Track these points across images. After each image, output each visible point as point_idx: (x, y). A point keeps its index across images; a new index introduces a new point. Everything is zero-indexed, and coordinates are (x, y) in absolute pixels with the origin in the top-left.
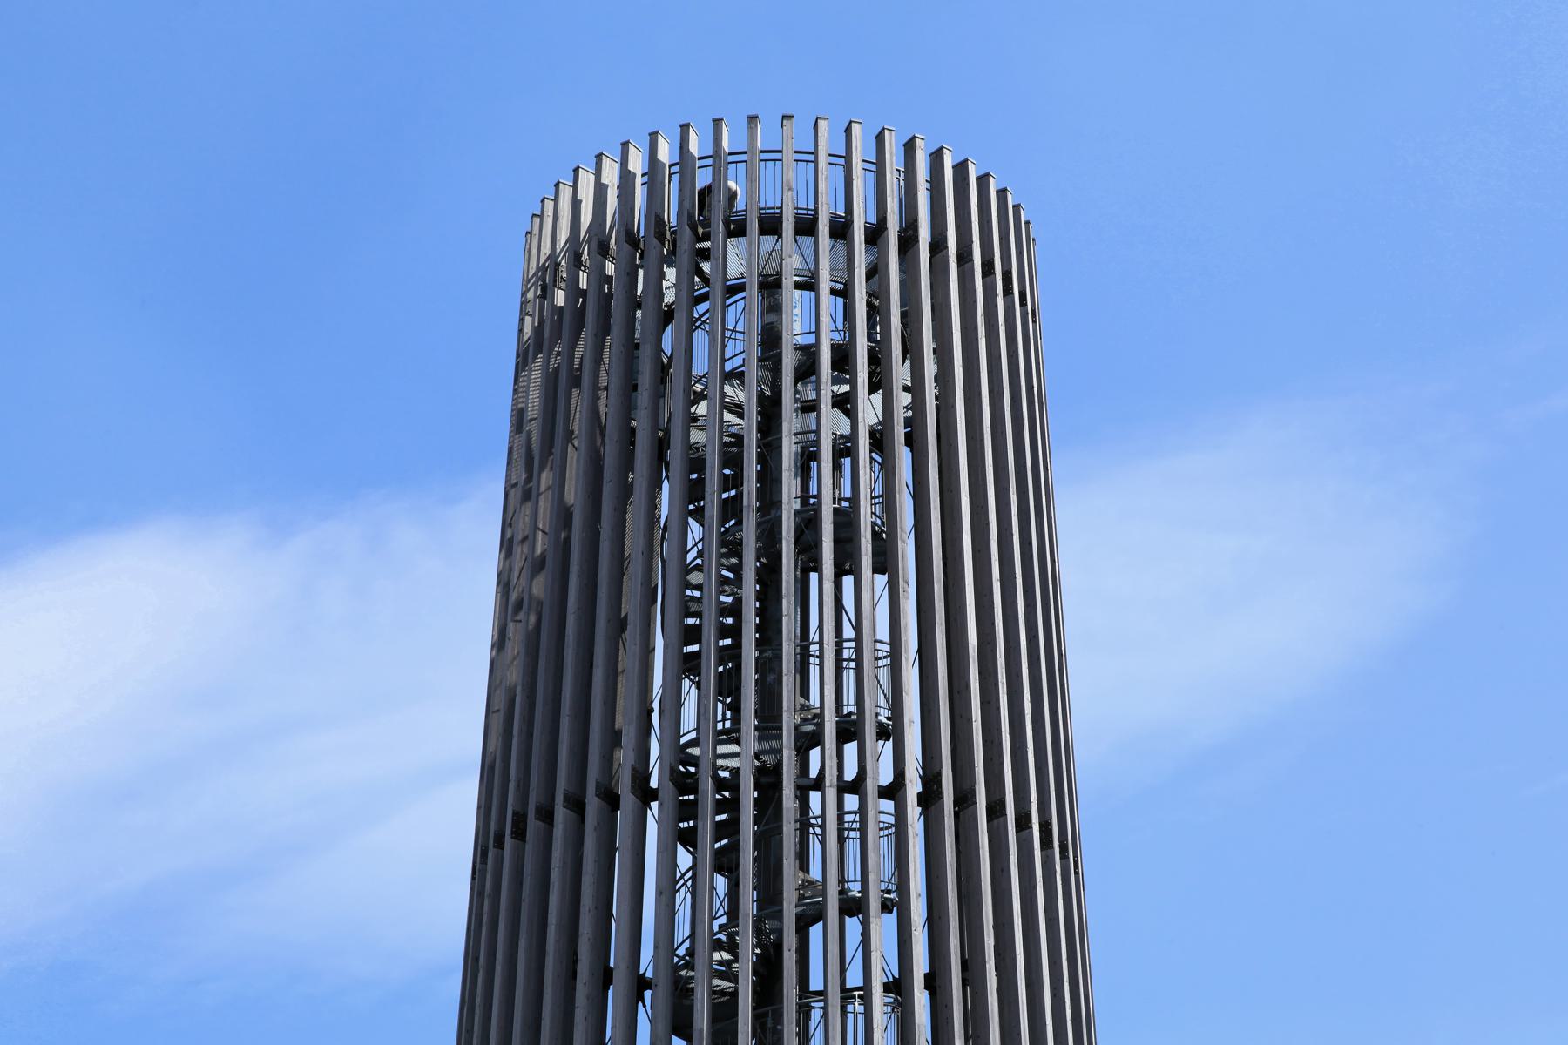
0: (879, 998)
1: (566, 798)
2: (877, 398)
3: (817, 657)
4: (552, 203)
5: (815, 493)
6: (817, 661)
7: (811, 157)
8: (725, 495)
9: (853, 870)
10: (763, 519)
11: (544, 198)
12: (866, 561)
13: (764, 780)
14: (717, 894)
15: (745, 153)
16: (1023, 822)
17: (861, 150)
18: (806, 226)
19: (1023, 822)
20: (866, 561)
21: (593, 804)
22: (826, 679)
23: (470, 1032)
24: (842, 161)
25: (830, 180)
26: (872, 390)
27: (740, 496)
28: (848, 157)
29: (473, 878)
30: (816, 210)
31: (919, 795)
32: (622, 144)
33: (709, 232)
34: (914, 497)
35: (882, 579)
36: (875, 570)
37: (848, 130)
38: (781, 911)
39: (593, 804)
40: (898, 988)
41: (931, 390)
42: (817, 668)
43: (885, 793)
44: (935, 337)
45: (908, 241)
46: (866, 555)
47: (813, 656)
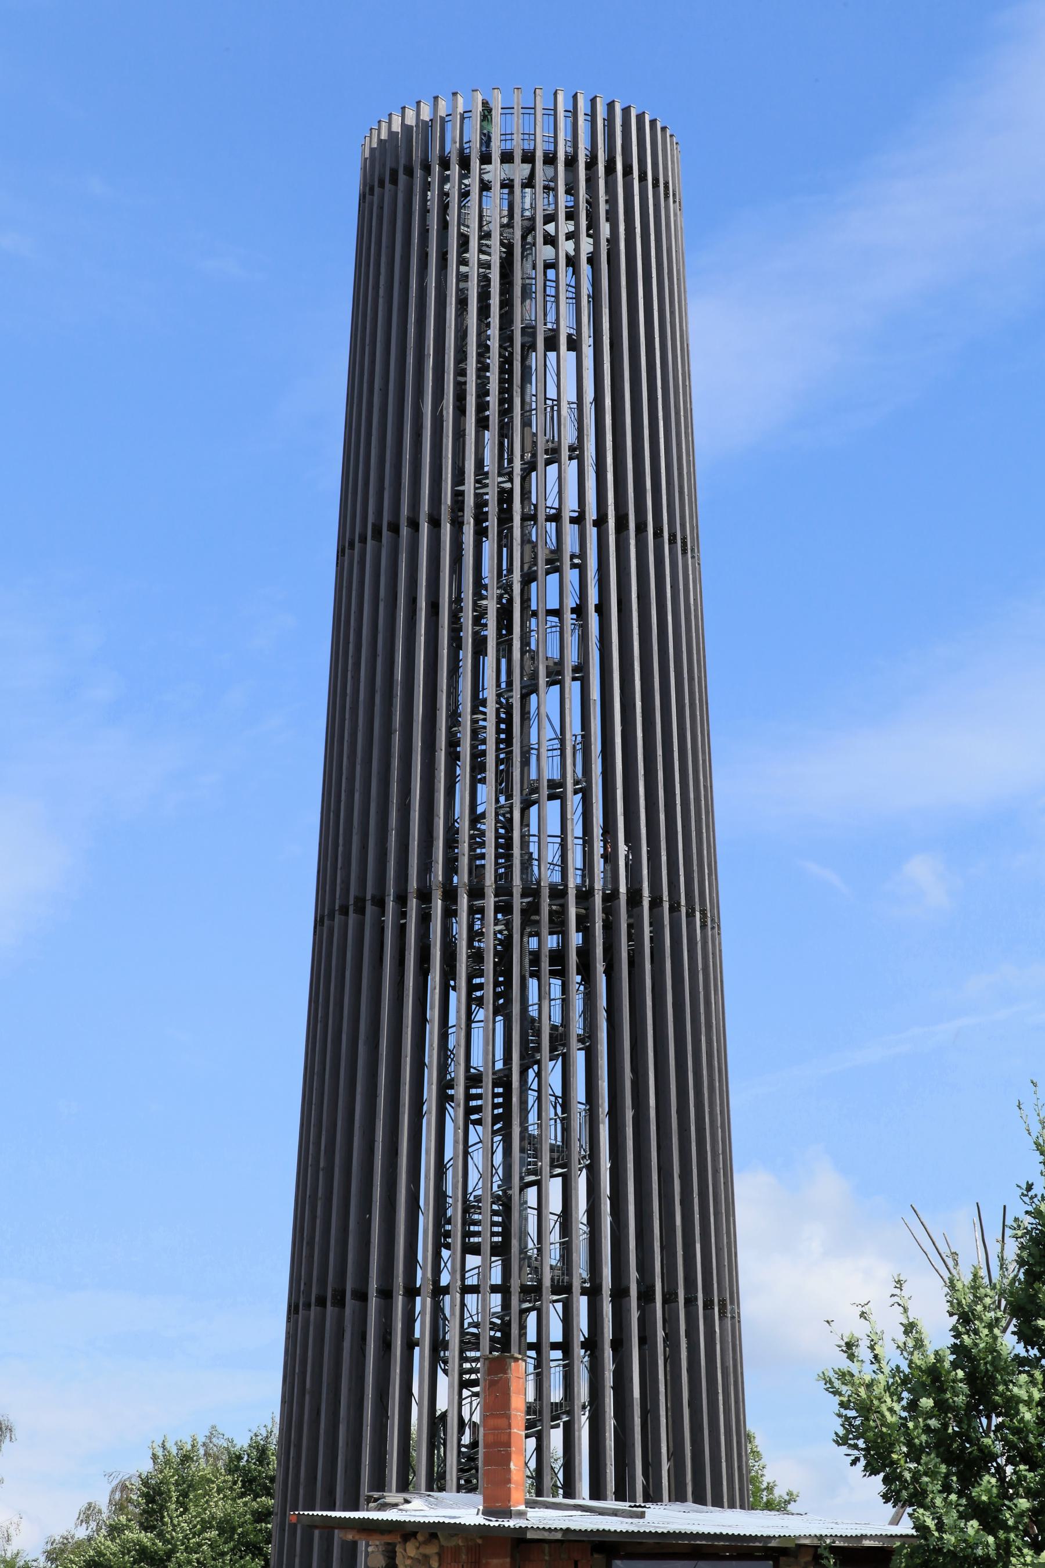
0: (569, 617)
2: (575, 462)
3: (536, 749)
7: (532, 111)
9: (552, 317)
13: (503, 516)
14: (468, 1310)
15: (482, 1021)
16: (643, 178)
18: (529, 158)
19: (643, 178)
22: (537, 122)
23: (330, 794)
24: (552, 112)
28: (555, 110)
29: (337, 566)
30: (535, 149)
31: (596, 605)
33: (469, 190)
34: (600, 650)
37: (555, 94)
40: (580, 611)
44: (607, 192)
45: (591, 164)
46: (568, 675)
47: (532, 749)
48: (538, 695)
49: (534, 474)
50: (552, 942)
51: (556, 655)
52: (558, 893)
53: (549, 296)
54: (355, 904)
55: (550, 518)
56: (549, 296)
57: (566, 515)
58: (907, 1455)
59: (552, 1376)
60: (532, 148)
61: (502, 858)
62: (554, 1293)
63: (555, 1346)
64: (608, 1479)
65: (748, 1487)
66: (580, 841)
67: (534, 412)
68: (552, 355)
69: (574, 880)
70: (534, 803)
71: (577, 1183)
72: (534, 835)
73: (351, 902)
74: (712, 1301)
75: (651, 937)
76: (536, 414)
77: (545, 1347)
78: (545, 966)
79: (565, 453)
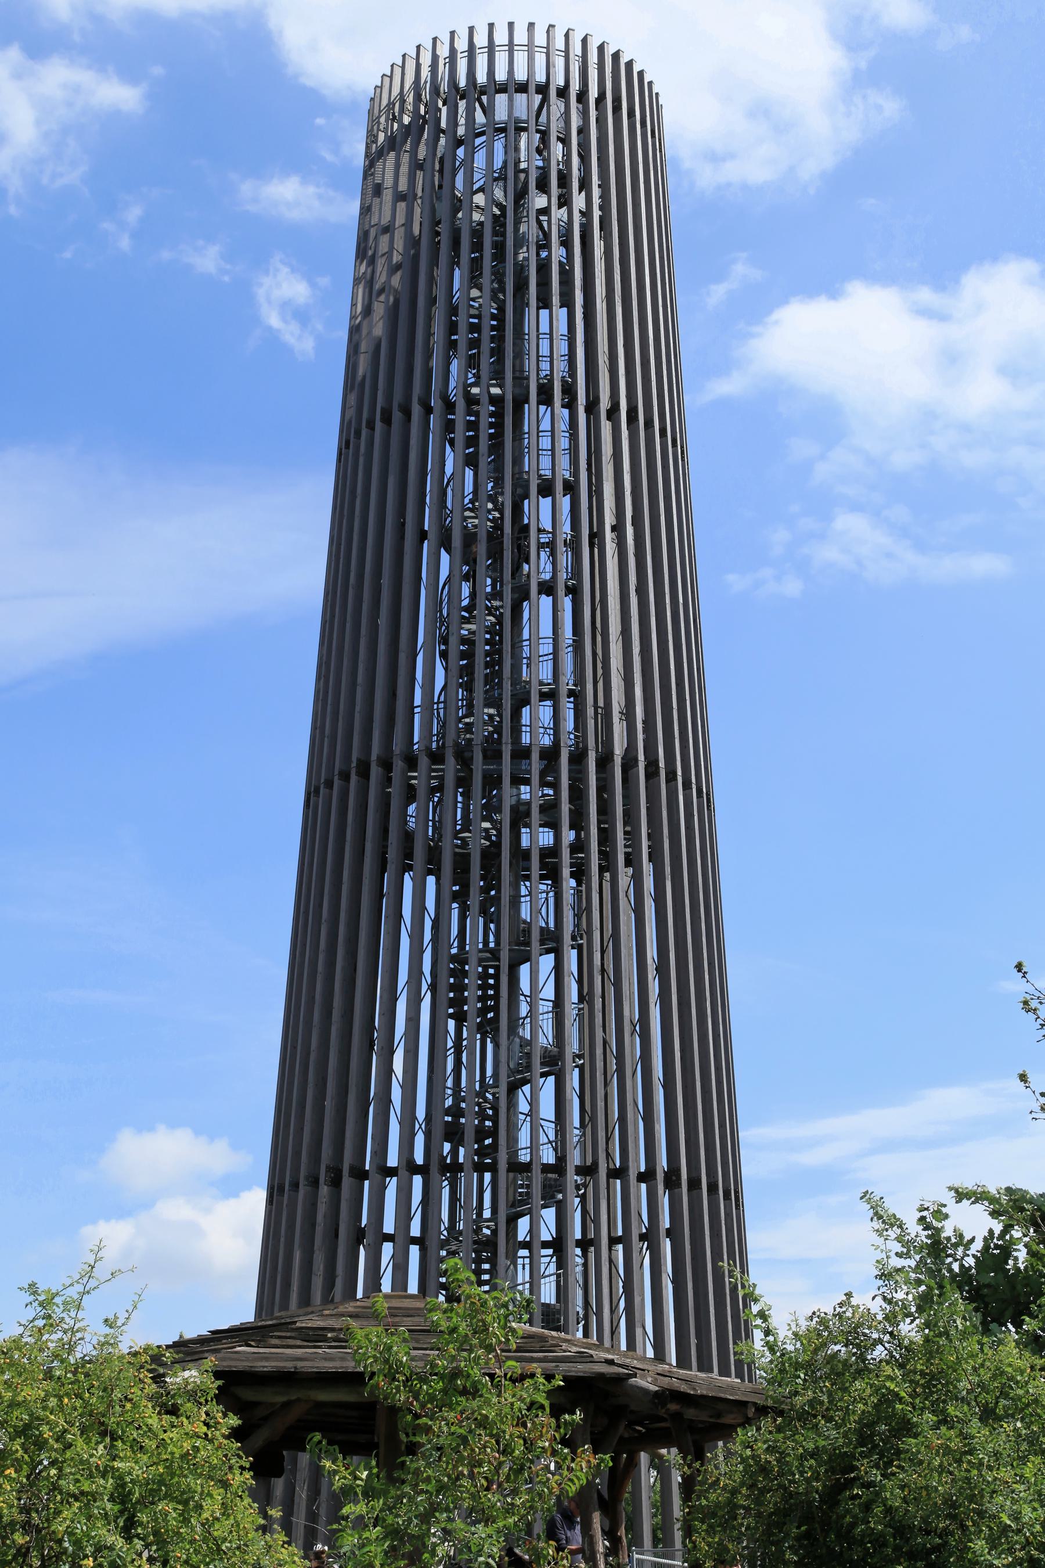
1: (400, 406)
4: (388, 79)
5: (527, 470)
6: (528, 729)
8: (473, 256)
10: (393, 1293)
11: (384, 75)
12: (556, 300)
17: (540, 39)
20: (556, 300)
21: (416, 410)
25: (564, 462)
26: (560, 207)
27: (482, 256)
32: (451, 32)
35: (630, 871)
36: (626, 866)
38: (499, 1027)
39: (416, 410)
41: (597, 213)
42: (528, 734)
43: (642, 1178)
48: (530, 602)
49: (526, 502)
50: (546, 838)
51: (544, 80)
52: (550, 755)
53: (542, 356)
54: (358, 766)
55: (543, 696)
56: (542, 356)
57: (563, 691)
58: (927, 1254)
59: (543, 1287)
60: (528, 1160)
61: (488, 1138)
62: (543, 1064)
63: (545, 1245)
64: (591, 800)
65: (755, 1372)
66: (567, 435)
67: (526, 436)
68: (544, 313)
69: (568, 742)
70: (525, 1082)
71: (573, 1218)
72: (526, 726)
73: (354, 764)
74: (691, 783)
75: (649, 853)
76: (529, 438)
77: (536, 1245)
78: (535, 870)
79: (559, 487)
